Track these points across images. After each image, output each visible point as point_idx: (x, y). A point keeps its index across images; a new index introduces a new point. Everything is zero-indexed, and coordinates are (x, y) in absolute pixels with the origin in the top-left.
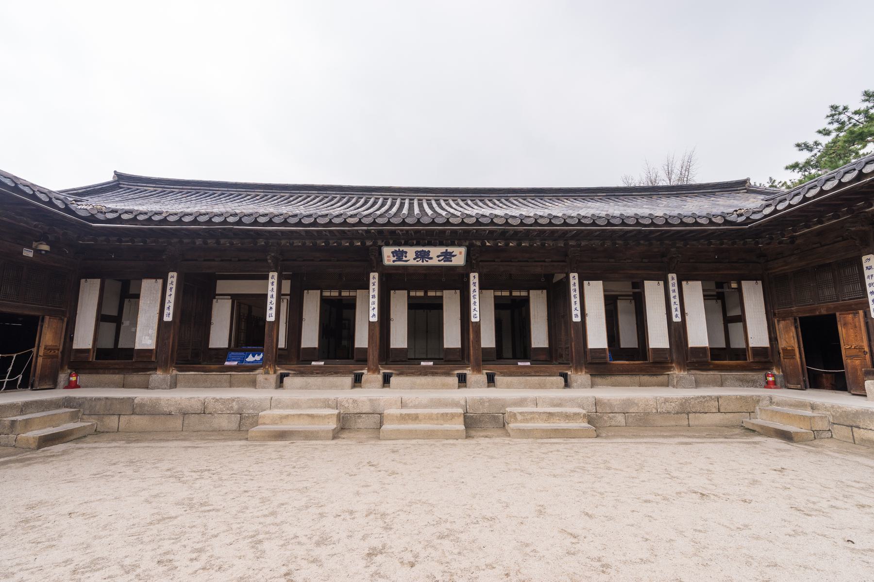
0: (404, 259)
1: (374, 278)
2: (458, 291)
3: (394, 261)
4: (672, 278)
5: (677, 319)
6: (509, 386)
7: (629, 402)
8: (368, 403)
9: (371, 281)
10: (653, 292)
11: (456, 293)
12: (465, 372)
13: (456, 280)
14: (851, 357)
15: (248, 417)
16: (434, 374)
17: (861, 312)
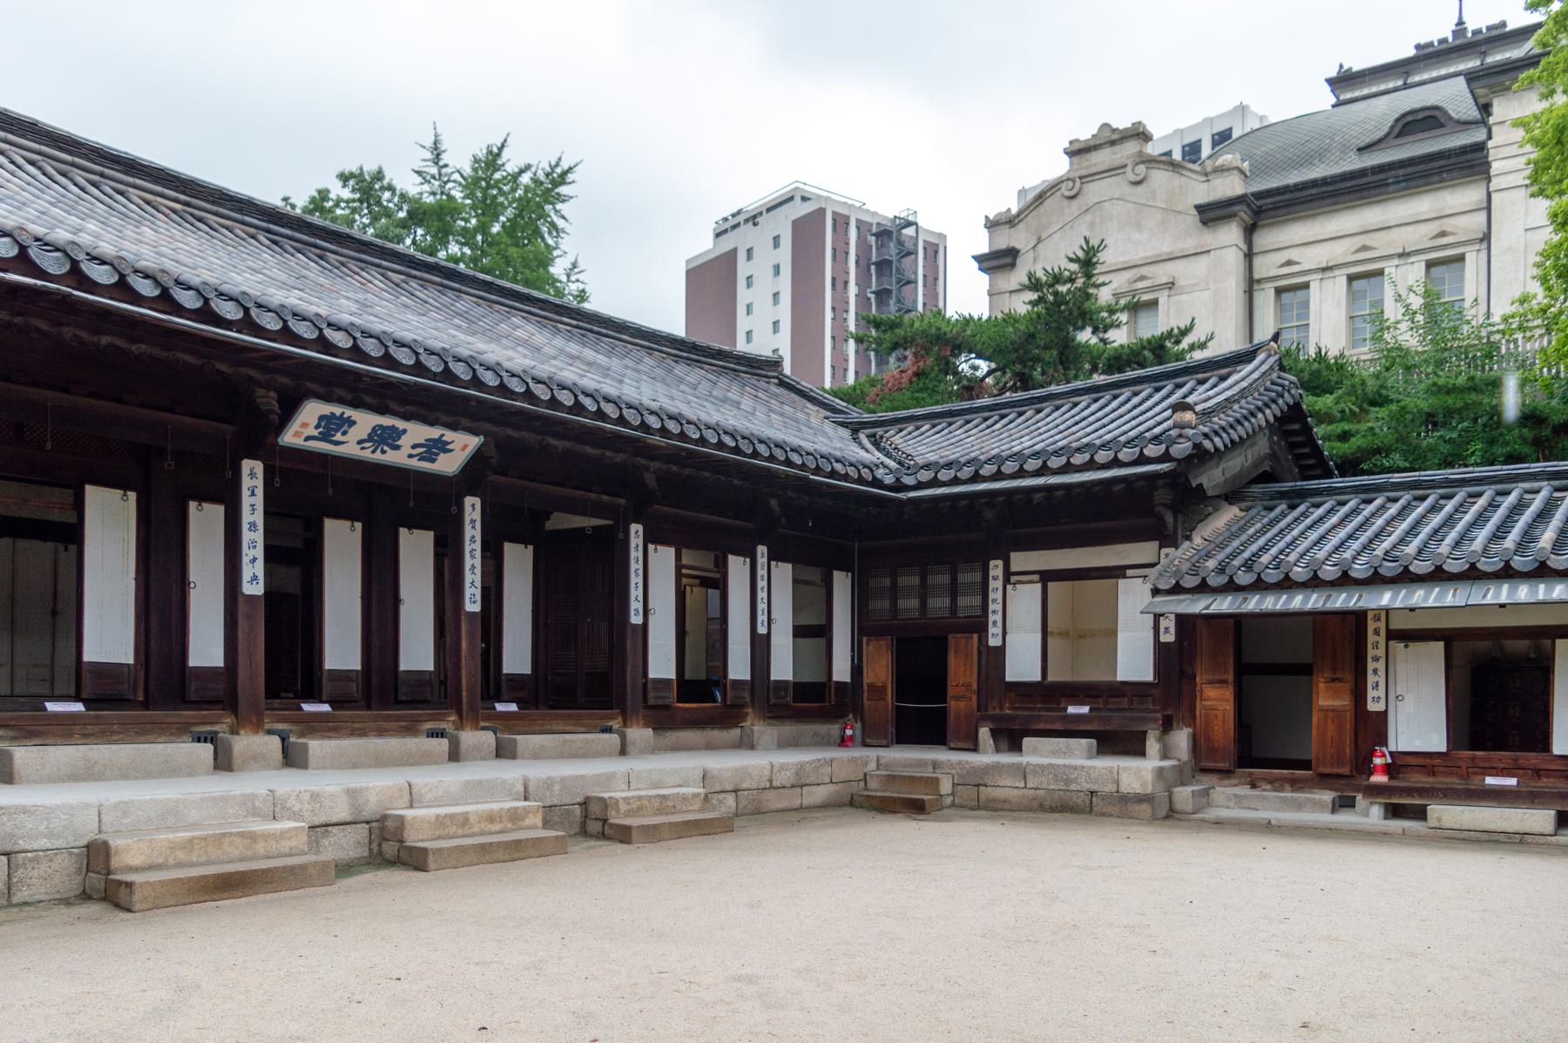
0: (338, 437)
1: (252, 475)
2: (358, 525)
3: (308, 439)
4: (762, 550)
5: (762, 630)
6: (537, 755)
7: (1052, 766)
8: (344, 798)
9: (246, 483)
10: (737, 567)
11: (125, 498)
12: (216, 728)
13: (430, 503)
14: (957, 698)
15: (36, 860)
16: (88, 737)
17: (975, 636)
